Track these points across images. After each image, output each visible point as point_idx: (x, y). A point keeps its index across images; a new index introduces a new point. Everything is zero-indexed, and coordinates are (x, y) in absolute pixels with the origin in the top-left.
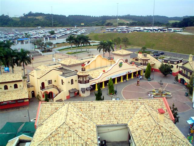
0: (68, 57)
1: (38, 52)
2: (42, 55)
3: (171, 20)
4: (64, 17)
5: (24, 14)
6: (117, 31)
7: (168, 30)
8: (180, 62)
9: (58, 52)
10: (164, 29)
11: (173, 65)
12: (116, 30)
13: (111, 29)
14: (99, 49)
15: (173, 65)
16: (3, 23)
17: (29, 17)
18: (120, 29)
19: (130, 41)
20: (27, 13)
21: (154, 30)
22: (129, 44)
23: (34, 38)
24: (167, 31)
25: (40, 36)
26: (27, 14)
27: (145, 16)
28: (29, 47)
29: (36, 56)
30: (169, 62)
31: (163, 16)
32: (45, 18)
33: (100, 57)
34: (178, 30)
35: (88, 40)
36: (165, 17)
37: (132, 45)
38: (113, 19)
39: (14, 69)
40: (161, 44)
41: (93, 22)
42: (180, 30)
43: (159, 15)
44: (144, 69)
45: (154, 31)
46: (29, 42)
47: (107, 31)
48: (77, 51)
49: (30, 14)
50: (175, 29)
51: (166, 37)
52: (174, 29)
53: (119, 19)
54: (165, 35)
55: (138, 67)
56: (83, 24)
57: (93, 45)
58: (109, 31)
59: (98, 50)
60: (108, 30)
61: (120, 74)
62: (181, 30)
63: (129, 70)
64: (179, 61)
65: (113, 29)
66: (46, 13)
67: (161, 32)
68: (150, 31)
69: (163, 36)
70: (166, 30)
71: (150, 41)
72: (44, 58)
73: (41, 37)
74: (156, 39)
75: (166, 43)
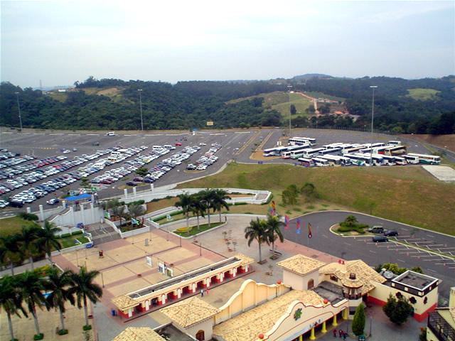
0: (181, 246)
1: (111, 229)
2: (122, 236)
3: (414, 88)
4: (167, 86)
5: (76, 83)
6: (288, 156)
7: (406, 158)
8: (430, 289)
9: (156, 224)
10: (397, 157)
11: (416, 298)
12: (287, 155)
13: (275, 150)
14: (249, 238)
15: (416, 298)
16: (31, 112)
17: (89, 92)
18: (296, 153)
19: (318, 189)
20: (82, 80)
21: (374, 159)
22: (318, 197)
23: (101, 182)
24: (403, 163)
25: (115, 177)
26: (83, 82)
27: (355, 78)
28: (93, 214)
29: (107, 239)
30: (406, 289)
31: (395, 78)
32: (125, 92)
33: (252, 285)
34: (429, 158)
35: (224, 198)
36: (400, 79)
37: (325, 200)
38: (280, 90)
39: (65, 314)
40: (389, 202)
41: (232, 102)
42: (433, 161)
43: (386, 76)
44: (350, 307)
45: (375, 161)
46: (92, 205)
47: (267, 155)
48: (198, 223)
49: (91, 83)
50: (422, 157)
51: (400, 186)
52: (420, 157)
53: (292, 92)
54: (399, 181)
55: (336, 305)
56: (210, 123)
57: (236, 204)
58: (271, 155)
59: (246, 237)
60: (268, 152)
61: (295, 334)
62: (438, 159)
63: (316, 320)
64: (429, 288)
65: (280, 151)
66: (126, 79)
67: (390, 164)
68: (364, 162)
69: (395, 183)
70: (401, 161)
71: (366, 194)
72: (128, 246)
73: (116, 179)
74: (379, 190)
75: (401, 201)
